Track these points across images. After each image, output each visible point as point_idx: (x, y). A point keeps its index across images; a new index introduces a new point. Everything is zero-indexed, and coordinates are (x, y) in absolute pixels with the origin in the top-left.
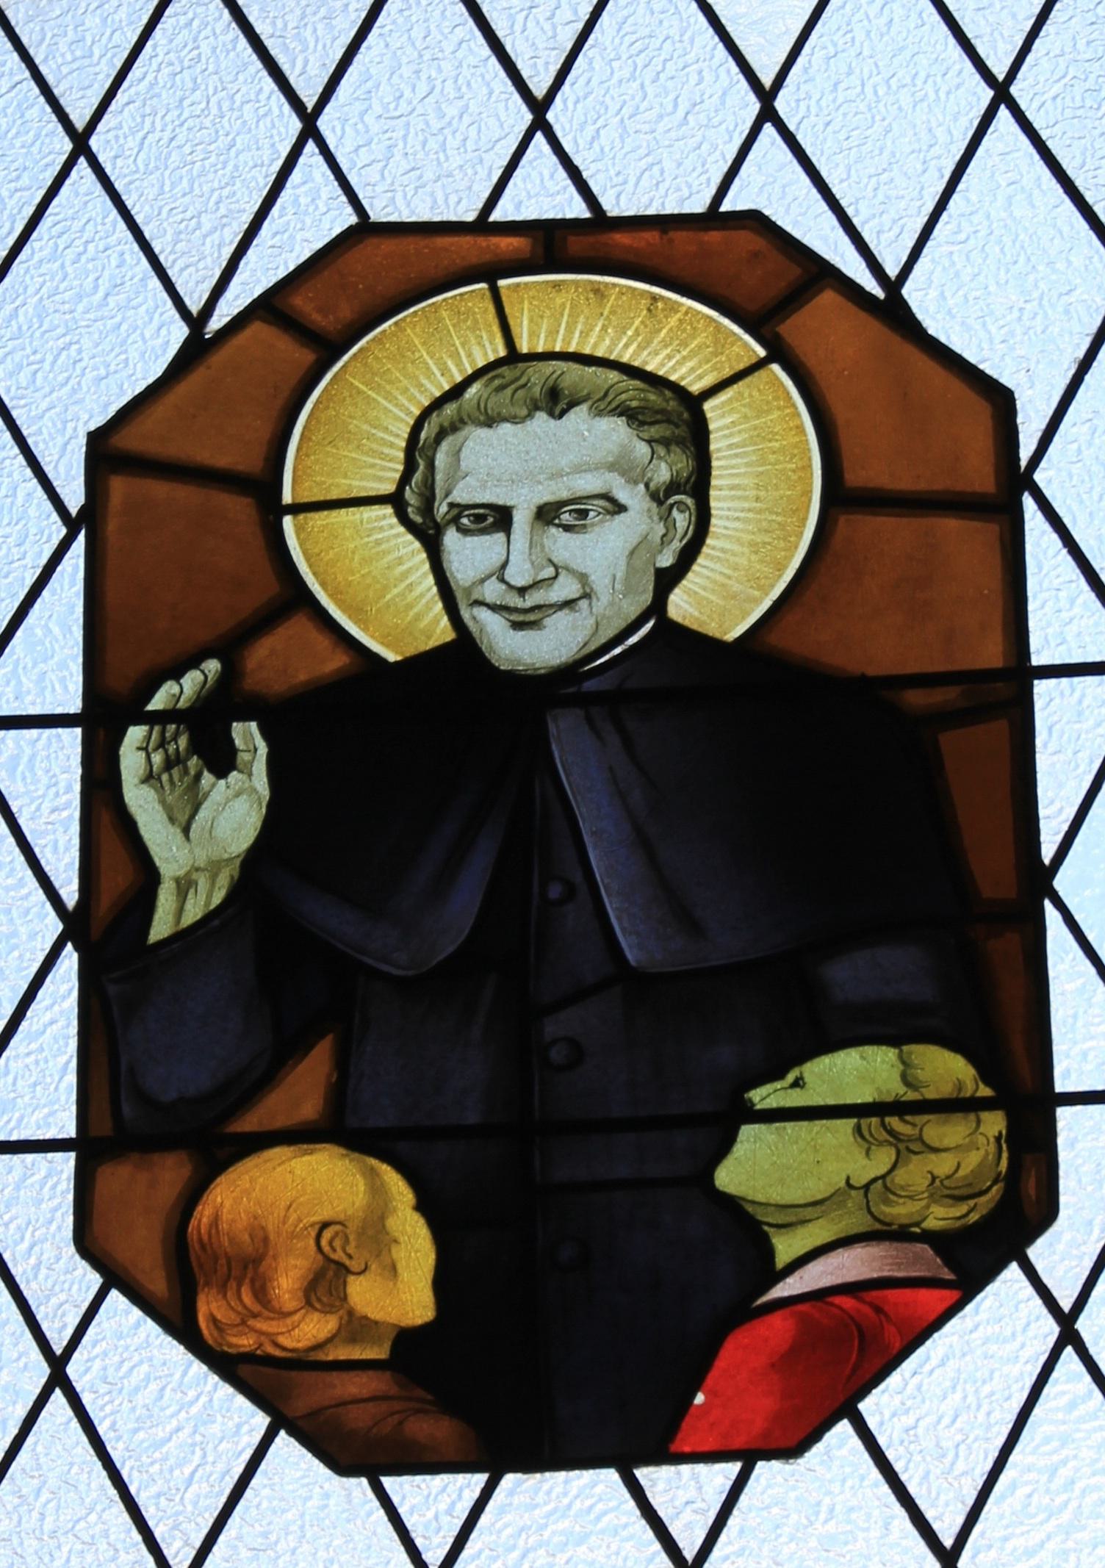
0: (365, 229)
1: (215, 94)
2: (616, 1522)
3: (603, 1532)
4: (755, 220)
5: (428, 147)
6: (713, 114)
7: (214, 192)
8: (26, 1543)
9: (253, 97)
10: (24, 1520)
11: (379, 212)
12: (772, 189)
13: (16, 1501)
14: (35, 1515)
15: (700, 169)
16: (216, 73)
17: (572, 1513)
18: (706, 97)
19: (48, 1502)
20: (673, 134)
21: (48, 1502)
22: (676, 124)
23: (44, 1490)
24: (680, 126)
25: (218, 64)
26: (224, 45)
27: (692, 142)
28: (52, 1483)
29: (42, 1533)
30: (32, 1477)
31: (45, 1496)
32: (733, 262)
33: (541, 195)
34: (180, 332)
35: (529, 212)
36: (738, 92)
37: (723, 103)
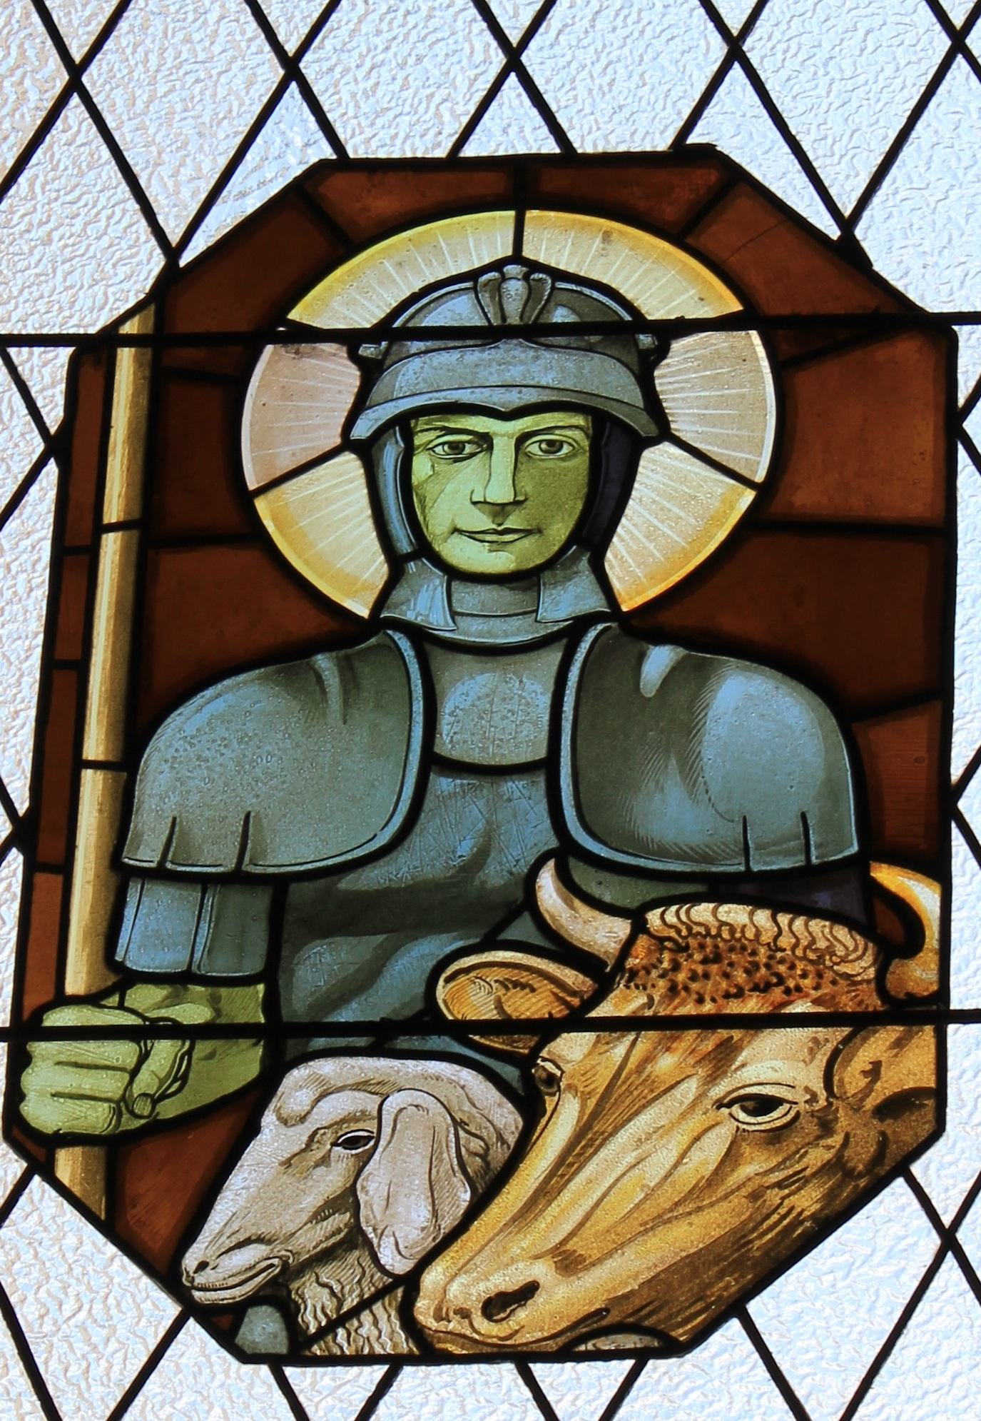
0: (342, 163)
1: (589, 133)
2: (702, 1399)
3: (690, 1407)
4: (708, 152)
5: (405, 90)
6: (582, 36)
7: (200, 135)
8: (93, 1388)
9: (628, 137)
10: (92, 1367)
11: (356, 149)
12: (736, 131)
13: (86, 1349)
14: (103, 1363)
15: (568, 87)
16: (592, 113)
17: (661, 1388)
18: (577, 19)
19: (116, 1351)
20: (546, 53)
21: (116, 1351)
22: (548, 43)
23: (113, 1339)
24: (552, 46)
25: (593, 105)
26: (601, 87)
27: (562, 62)
28: (121, 1332)
29: (109, 1380)
30: (104, 1327)
31: (113, 1345)
32: (685, 192)
33: (513, 132)
34: (158, 261)
35: (502, 148)
36: (608, 16)
37: (593, 27)
